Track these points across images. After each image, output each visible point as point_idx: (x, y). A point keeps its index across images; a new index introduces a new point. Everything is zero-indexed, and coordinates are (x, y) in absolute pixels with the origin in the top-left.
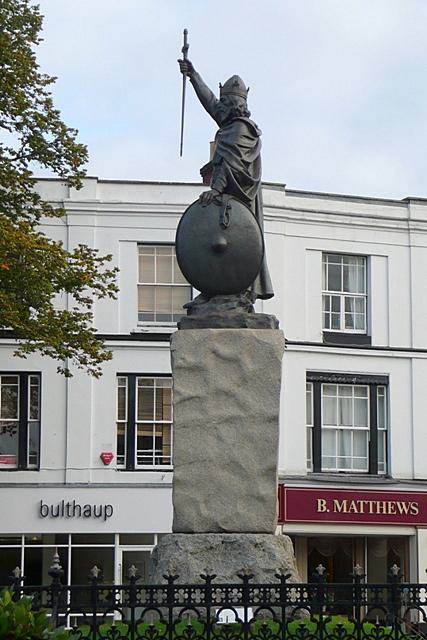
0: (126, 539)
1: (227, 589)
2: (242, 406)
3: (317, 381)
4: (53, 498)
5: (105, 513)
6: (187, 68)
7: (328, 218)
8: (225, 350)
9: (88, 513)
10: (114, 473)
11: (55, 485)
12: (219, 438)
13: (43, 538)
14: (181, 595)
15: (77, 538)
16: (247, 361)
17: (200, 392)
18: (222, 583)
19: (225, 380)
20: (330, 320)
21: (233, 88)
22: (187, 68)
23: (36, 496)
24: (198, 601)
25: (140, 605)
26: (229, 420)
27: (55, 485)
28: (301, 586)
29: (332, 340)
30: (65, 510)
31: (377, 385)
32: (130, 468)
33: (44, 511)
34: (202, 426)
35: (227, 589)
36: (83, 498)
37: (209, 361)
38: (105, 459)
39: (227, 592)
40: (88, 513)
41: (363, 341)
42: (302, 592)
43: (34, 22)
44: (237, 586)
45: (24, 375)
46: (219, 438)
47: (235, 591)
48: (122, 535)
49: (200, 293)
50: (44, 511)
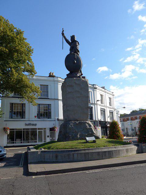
0: (39, 129)
4: (27, 122)
5: (36, 125)
6: (63, 34)
8: (77, 82)
9: (33, 125)
10: (36, 119)
11: (28, 121)
13: (26, 129)
15: (31, 129)
21: (73, 37)
22: (63, 34)
27: (28, 121)
30: (29, 124)
32: (39, 118)
33: (26, 125)
36: (32, 123)
38: (35, 117)
40: (33, 125)
43: (29, 51)
45: (23, 104)
48: (31, 129)
49: (69, 72)
50: (26, 125)
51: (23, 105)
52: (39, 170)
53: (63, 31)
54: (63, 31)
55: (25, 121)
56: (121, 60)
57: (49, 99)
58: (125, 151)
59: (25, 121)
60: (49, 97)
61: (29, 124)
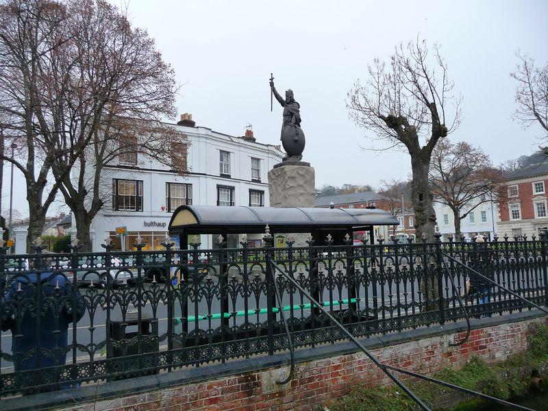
1: (208, 253)
2: (305, 190)
3: (219, 187)
4: (148, 220)
6: (272, 84)
7: (222, 141)
8: (301, 173)
9: (159, 225)
11: (148, 216)
12: (299, 200)
14: (296, 254)
15: (155, 233)
16: (306, 176)
17: (295, 185)
18: (300, 246)
19: (301, 183)
20: (221, 170)
21: (289, 94)
22: (272, 84)
23: (143, 220)
24: (284, 258)
25: (250, 262)
26: (302, 194)
27: (148, 216)
28: (208, 251)
29: (222, 176)
30: (152, 224)
31: (232, 189)
33: (146, 224)
34: (295, 195)
35: (208, 253)
36: (158, 220)
37: (297, 176)
39: (301, 253)
40: (159, 225)
41: (229, 177)
42: (208, 256)
44: (306, 248)
46: (299, 200)
47: (160, 256)
50: (146, 224)
51: (139, 183)
52: (369, 216)
53: (272, 79)
54: (272, 79)
55: (143, 216)
56: (544, 291)
57: (138, 168)
58: (210, 340)
59: (143, 216)
60: (189, 170)
61: (152, 224)
